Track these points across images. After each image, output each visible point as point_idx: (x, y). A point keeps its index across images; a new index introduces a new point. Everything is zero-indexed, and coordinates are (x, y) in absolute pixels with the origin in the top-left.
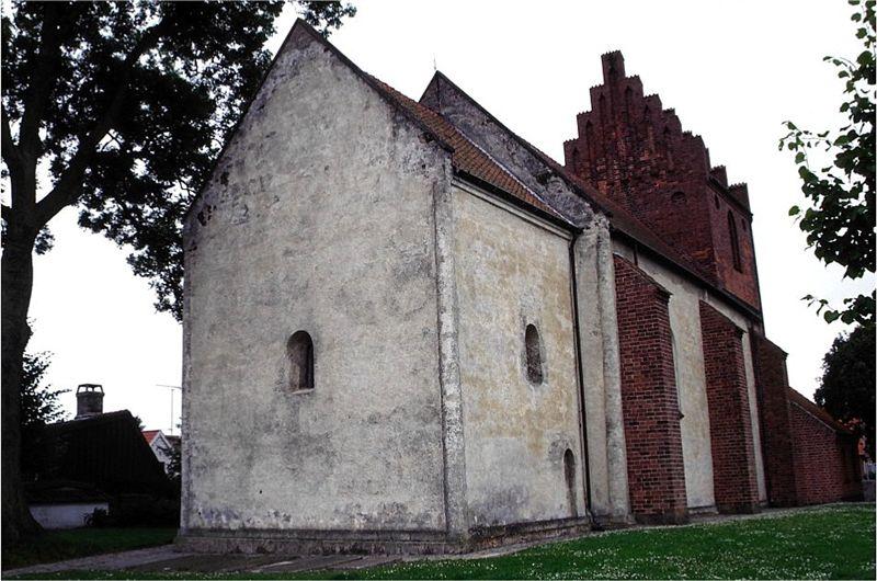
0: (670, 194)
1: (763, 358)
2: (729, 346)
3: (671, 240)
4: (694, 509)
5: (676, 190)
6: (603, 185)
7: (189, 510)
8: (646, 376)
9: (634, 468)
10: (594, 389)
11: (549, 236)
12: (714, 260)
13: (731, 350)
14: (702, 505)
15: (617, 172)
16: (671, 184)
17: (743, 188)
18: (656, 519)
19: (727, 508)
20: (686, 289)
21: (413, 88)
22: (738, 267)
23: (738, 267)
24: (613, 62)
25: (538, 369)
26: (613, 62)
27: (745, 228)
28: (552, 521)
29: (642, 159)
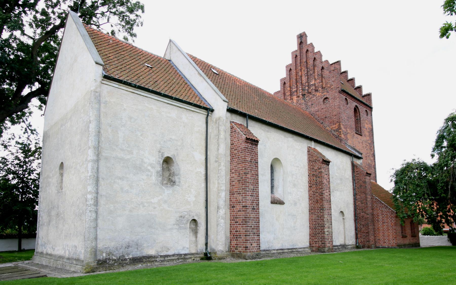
0: (323, 99)
1: (357, 175)
2: (319, 169)
3: (322, 121)
4: (264, 250)
5: (325, 97)
6: (295, 98)
7: (38, 244)
8: (239, 183)
9: (233, 229)
10: (213, 187)
11: (192, 112)
12: (340, 129)
13: (320, 170)
14: (297, 247)
15: (301, 91)
16: (323, 94)
17: (369, 95)
18: (239, 256)
19: (314, 249)
20: (285, 137)
21: (268, 74)
22: (359, 132)
23: (359, 132)
24: (302, 38)
25: (173, 179)
26: (302, 38)
27: (367, 115)
28: (173, 255)
29: (311, 83)
